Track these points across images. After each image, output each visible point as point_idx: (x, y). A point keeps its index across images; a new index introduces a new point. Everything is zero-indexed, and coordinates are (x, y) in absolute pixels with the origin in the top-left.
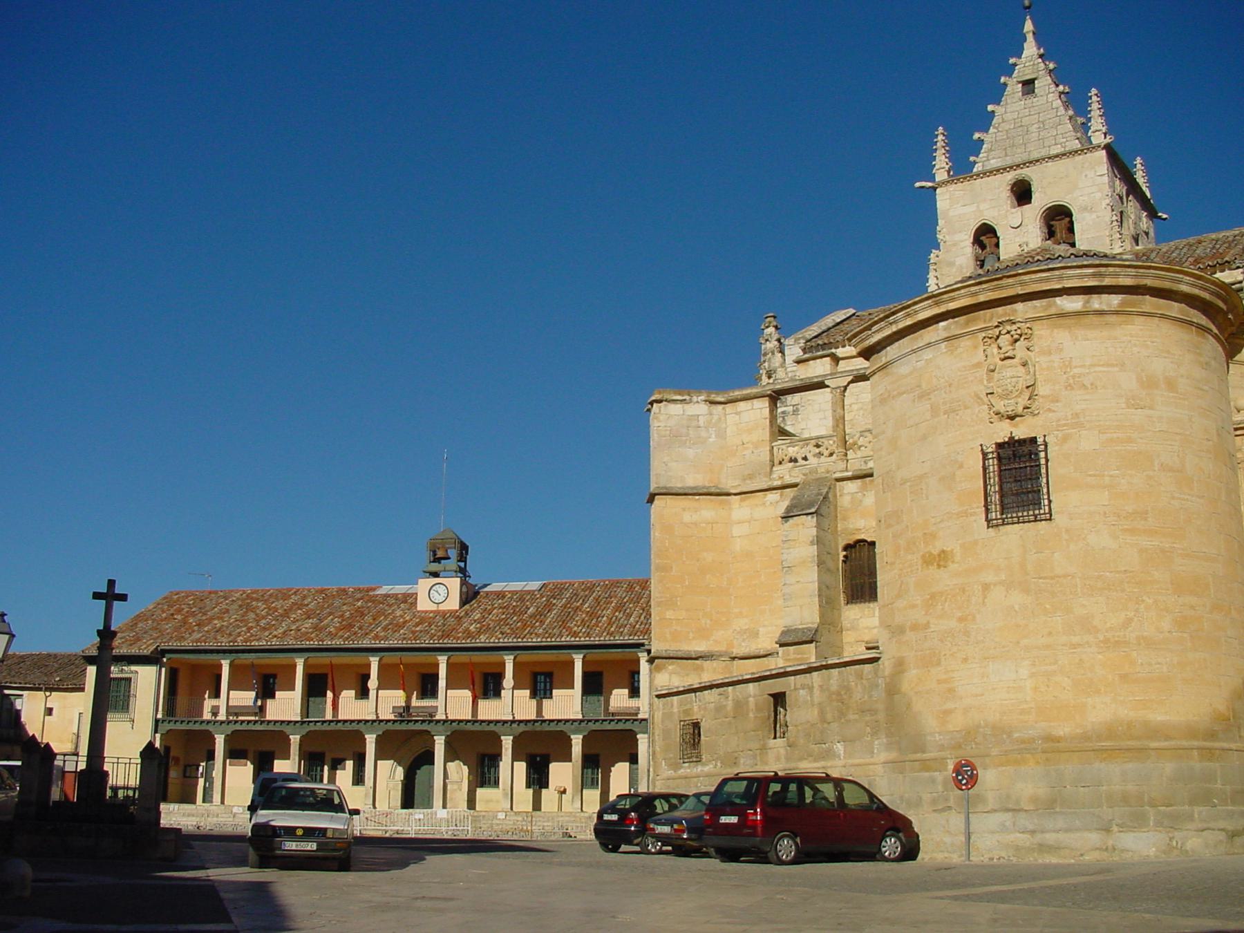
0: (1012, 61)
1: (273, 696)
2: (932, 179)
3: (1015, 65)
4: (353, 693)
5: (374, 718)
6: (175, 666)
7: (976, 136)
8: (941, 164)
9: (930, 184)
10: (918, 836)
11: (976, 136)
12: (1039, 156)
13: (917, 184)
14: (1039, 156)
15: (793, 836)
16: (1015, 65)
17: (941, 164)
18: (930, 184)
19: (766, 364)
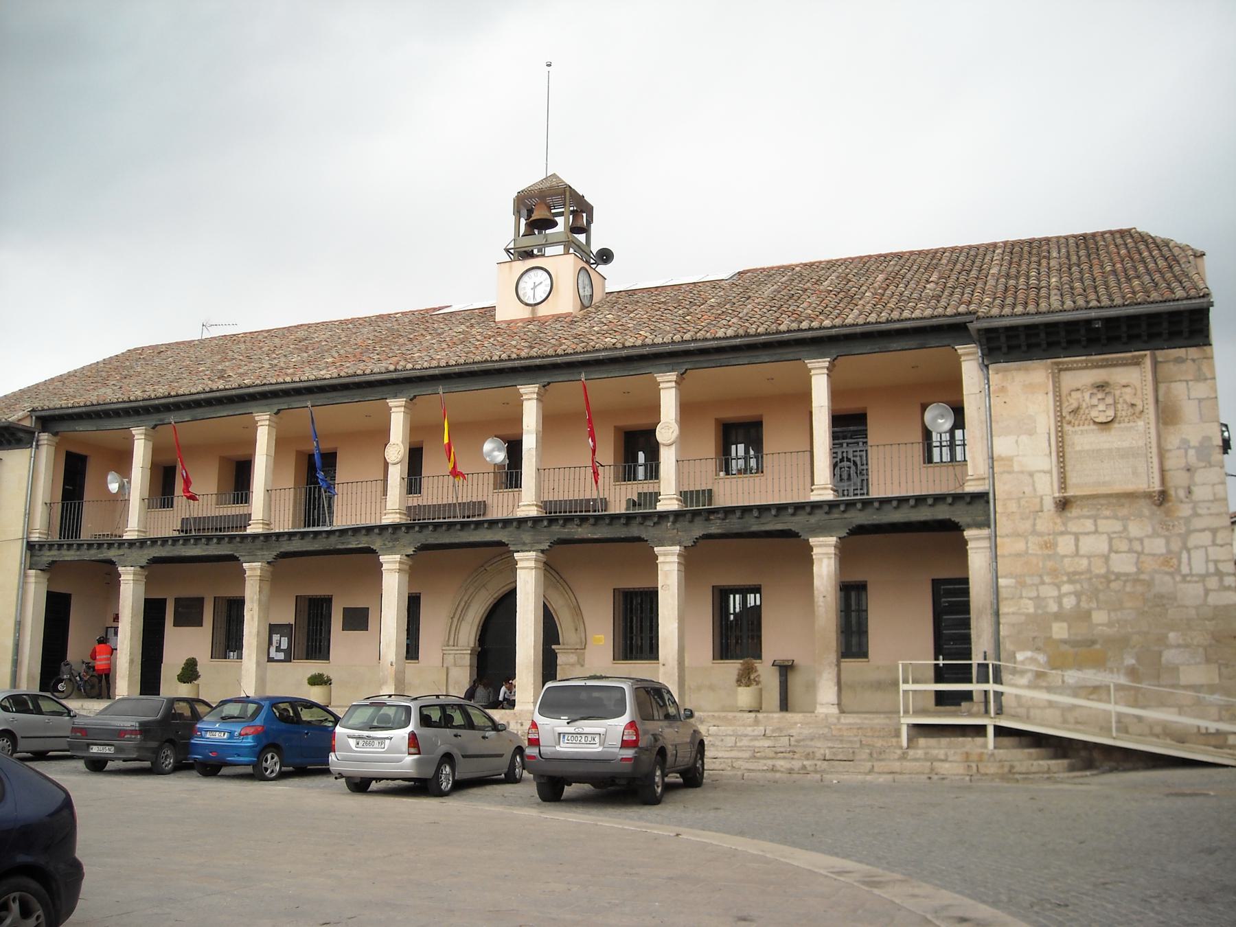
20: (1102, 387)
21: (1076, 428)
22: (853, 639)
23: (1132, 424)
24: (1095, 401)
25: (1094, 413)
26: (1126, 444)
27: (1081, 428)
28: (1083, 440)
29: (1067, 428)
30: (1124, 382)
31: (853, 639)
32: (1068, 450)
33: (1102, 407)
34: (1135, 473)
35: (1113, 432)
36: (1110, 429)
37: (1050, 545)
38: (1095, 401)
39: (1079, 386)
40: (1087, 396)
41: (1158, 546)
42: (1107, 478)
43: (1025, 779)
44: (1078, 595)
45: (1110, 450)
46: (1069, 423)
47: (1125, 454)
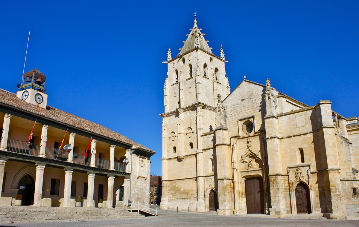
0: (180, 49)
1: (125, 157)
2: (167, 61)
3: (191, 30)
4: (331, 214)
5: (213, 178)
6: (102, 152)
7: (183, 42)
8: (169, 56)
9: (166, 62)
10: (261, 125)
11: (183, 42)
12: (197, 37)
13: (163, 62)
14: (197, 37)
15: (25, 188)
16: (191, 30)
17: (169, 56)
18: (166, 62)
19: (94, 209)
37: (136, 183)
41: (144, 185)
44: (138, 191)
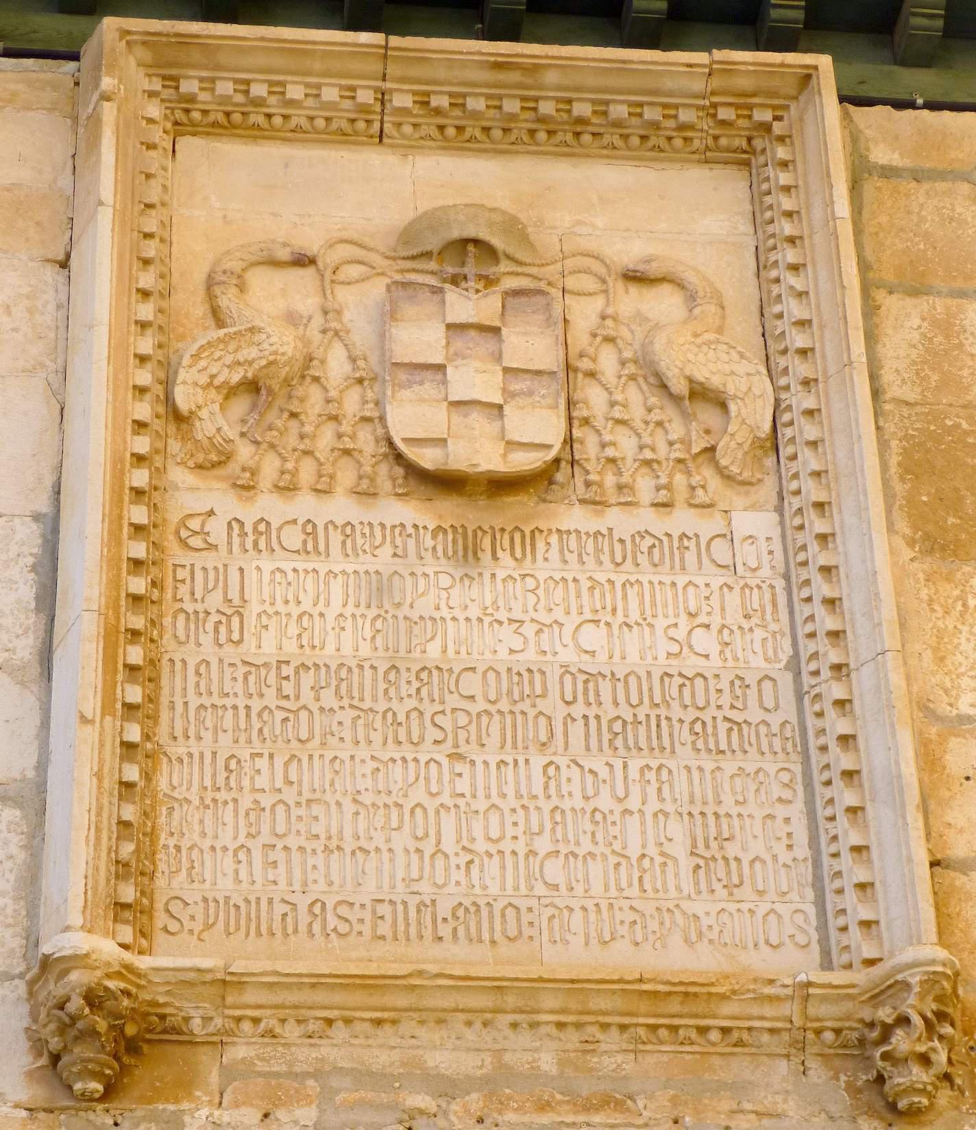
20: (464, 254)
21: (269, 506)
22: (495, 557)
23: (682, 520)
24: (419, 337)
25: (412, 417)
26: (642, 651)
27: (305, 506)
28: (301, 581)
29: (192, 495)
30: (630, 252)
31: (495, 557)
32: (190, 651)
33: (474, 379)
34: (712, 858)
35: (547, 563)
36: (526, 540)
38: (419, 337)
39: (311, 242)
40: (359, 303)
42: (493, 881)
43: (313, 985)
45: (523, 682)
46: (214, 461)
47: (641, 719)
